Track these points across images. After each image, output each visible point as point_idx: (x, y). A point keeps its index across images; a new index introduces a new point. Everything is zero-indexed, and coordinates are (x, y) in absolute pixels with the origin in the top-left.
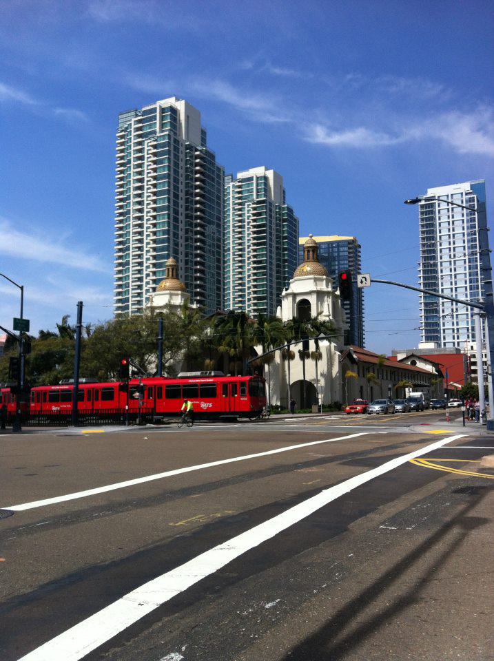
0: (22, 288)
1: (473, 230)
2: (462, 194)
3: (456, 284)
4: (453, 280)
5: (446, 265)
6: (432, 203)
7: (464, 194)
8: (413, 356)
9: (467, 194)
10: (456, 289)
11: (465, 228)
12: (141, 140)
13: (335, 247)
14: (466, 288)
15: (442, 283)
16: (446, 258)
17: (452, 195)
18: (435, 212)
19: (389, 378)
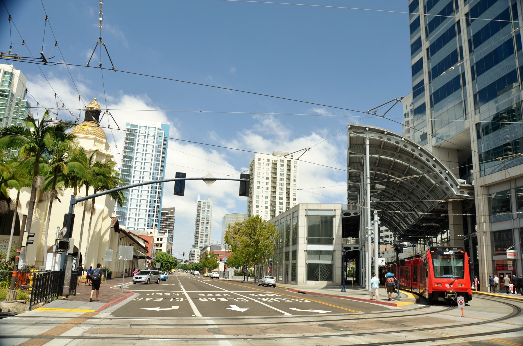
2: (155, 128)
5: (141, 146)
6: (135, 130)
7: (157, 129)
9: (158, 129)
10: (147, 145)
11: (153, 160)
14: (148, 191)
15: (131, 204)
17: (149, 127)
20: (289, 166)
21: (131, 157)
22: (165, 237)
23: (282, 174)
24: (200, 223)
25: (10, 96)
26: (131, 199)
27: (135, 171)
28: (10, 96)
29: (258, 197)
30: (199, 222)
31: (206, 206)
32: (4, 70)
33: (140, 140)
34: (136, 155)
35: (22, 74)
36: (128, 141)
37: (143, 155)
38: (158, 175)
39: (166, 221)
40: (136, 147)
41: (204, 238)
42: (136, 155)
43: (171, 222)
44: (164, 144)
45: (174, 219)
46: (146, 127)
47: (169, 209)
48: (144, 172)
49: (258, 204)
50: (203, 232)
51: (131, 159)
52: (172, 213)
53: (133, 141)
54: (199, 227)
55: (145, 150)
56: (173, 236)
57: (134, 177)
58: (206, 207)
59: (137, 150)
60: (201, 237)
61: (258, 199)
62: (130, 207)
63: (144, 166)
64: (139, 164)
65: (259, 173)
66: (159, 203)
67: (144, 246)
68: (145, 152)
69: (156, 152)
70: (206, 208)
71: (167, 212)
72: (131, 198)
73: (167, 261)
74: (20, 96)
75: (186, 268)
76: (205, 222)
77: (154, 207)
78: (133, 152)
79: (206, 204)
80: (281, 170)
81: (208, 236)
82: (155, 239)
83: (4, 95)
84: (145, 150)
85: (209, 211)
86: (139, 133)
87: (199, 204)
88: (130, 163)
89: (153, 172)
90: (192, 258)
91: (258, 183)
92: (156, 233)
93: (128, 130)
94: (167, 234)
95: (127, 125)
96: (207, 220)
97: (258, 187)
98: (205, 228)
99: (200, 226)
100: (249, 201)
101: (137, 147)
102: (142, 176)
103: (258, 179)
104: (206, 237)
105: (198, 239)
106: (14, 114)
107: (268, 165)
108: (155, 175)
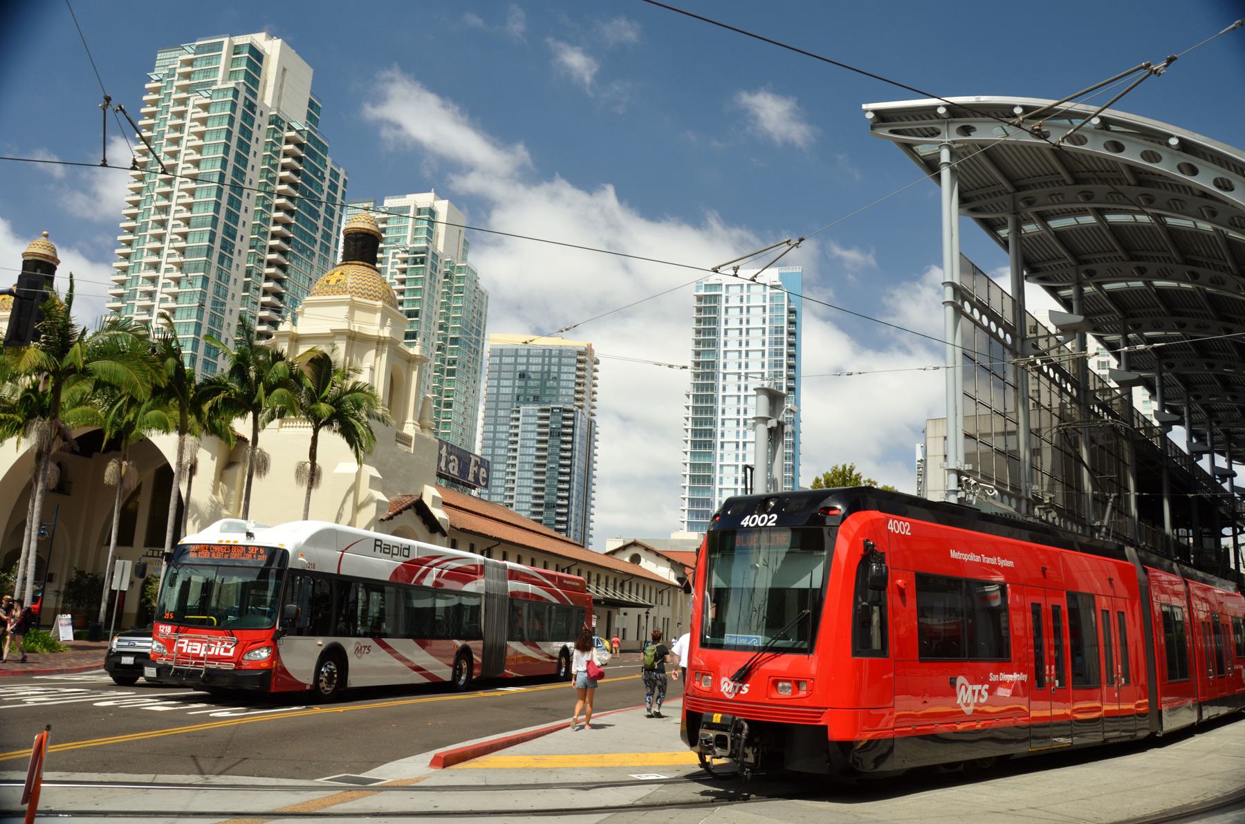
2: (765, 285)
3: (748, 301)
6: (716, 296)
8: (635, 544)
9: (772, 287)
12: (184, 95)
13: (554, 365)
15: (721, 479)
16: (734, 323)
18: (718, 344)
21: (712, 364)
25: (430, 259)
26: (721, 466)
27: (724, 397)
28: (430, 259)
32: (415, 206)
33: (730, 320)
35: (451, 204)
36: (702, 327)
37: (740, 357)
40: (720, 406)
42: (725, 357)
44: (791, 323)
51: (712, 390)
53: (713, 379)
55: (744, 321)
57: (723, 412)
59: (726, 322)
62: (721, 487)
63: (747, 360)
64: (734, 313)
68: (744, 348)
69: (770, 343)
72: (722, 463)
74: (452, 257)
78: (717, 350)
83: (418, 260)
84: (744, 321)
88: (713, 367)
93: (699, 299)
95: (698, 288)
102: (742, 407)
106: (442, 298)
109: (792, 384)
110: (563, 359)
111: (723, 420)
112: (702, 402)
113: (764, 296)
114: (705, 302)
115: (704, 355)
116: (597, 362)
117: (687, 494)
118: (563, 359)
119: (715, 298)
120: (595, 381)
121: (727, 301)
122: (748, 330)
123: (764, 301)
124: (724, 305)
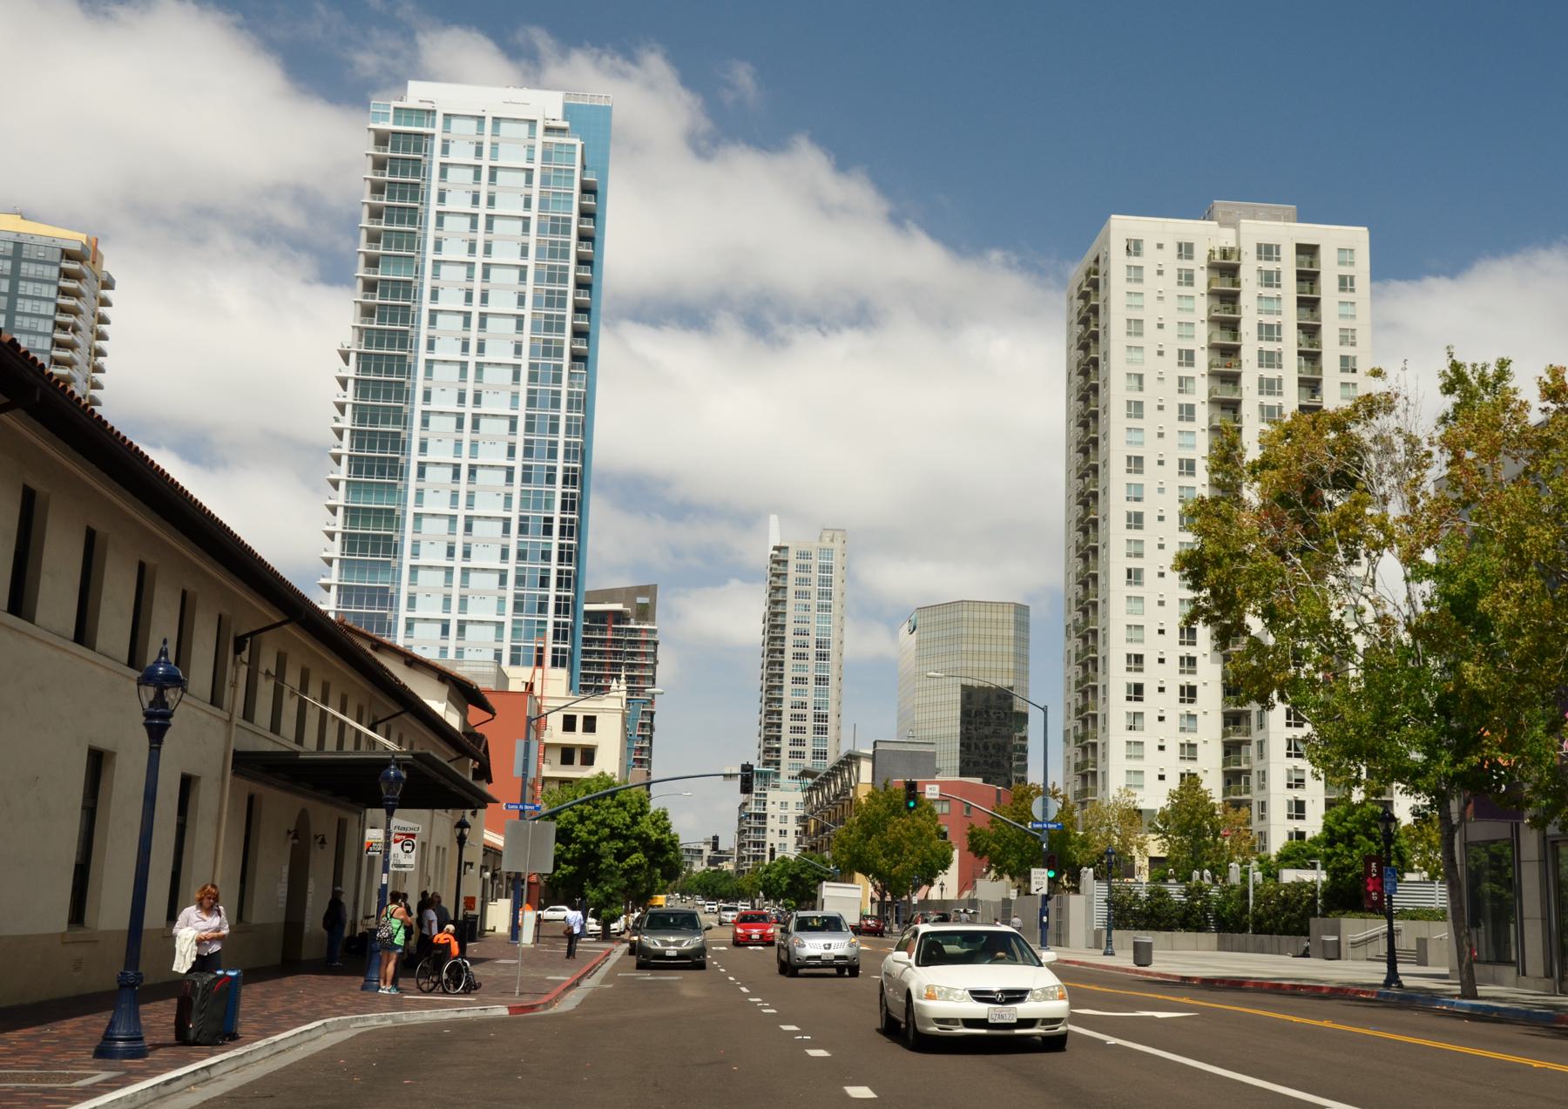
0: (1045, 710)
1: (558, 263)
2: (532, 123)
3: (494, 156)
4: (456, 592)
9: (548, 130)
14: (510, 472)
15: (416, 545)
16: (448, 349)
17: (497, 120)
19: (114, 626)
20: (1308, 277)
21: (406, 289)
22: (610, 707)
23: (1270, 327)
24: (788, 656)
29: (1136, 464)
30: (782, 652)
31: (815, 569)
34: (436, 275)
37: (470, 277)
38: (557, 379)
39: (615, 653)
40: (424, 331)
41: (809, 736)
42: (436, 275)
43: (639, 660)
44: (586, 213)
45: (656, 644)
46: (481, 119)
47: (627, 594)
48: (480, 366)
49: (1135, 507)
50: (803, 705)
51: (403, 345)
52: (645, 613)
54: (781, 676)
55: (480, 248)
56: (652, 729)
58: (815, 574)
60: (795, 730)
61: (1135, 478)
65: (1135, 327)
66: (571, 534)
67: (454, 720)
69: (536, 302)
70: (815, 581)
71: (618, 607)
72: (419, 510)
73: (625, 838)
75: (725, 887)
76: (812, 651)
77: (546, 556)
79: (815, 563)
80: (1265, 305)
81: (832, 723)
82: (555, 722)
84: (480, 248)
85: (828, 595)
86: (471, 266)
87: (778, 562)
88: (416, 173)
89: (532, 366)
90: (753, 836)
91: (1135, 383)
92: (555, 685)
94: (619, 689)
96: (819, 644)
97: (1136, 409)
98: (811, 681)
99: (789, 672)
100: (1080, 494)
101: (439, 234)
103: (1129, 361)
104: (822, 730)
105: (778, 739)
107: (1187, 278)
108: (545, 380)
109: (588, 226)
110: (24, 266)
111: (426, 415)
112: (378, 371)
113: (531, 149)
114: (395, 149)
115: (387, 265)
116: (108, 284)
117: (340, 498)
118: (24, 266)
119: (420, 141)
120: (103, 327)
121: (445, 150)
122: (483, 317)
123: (530, 159)
124: (437, 158)
